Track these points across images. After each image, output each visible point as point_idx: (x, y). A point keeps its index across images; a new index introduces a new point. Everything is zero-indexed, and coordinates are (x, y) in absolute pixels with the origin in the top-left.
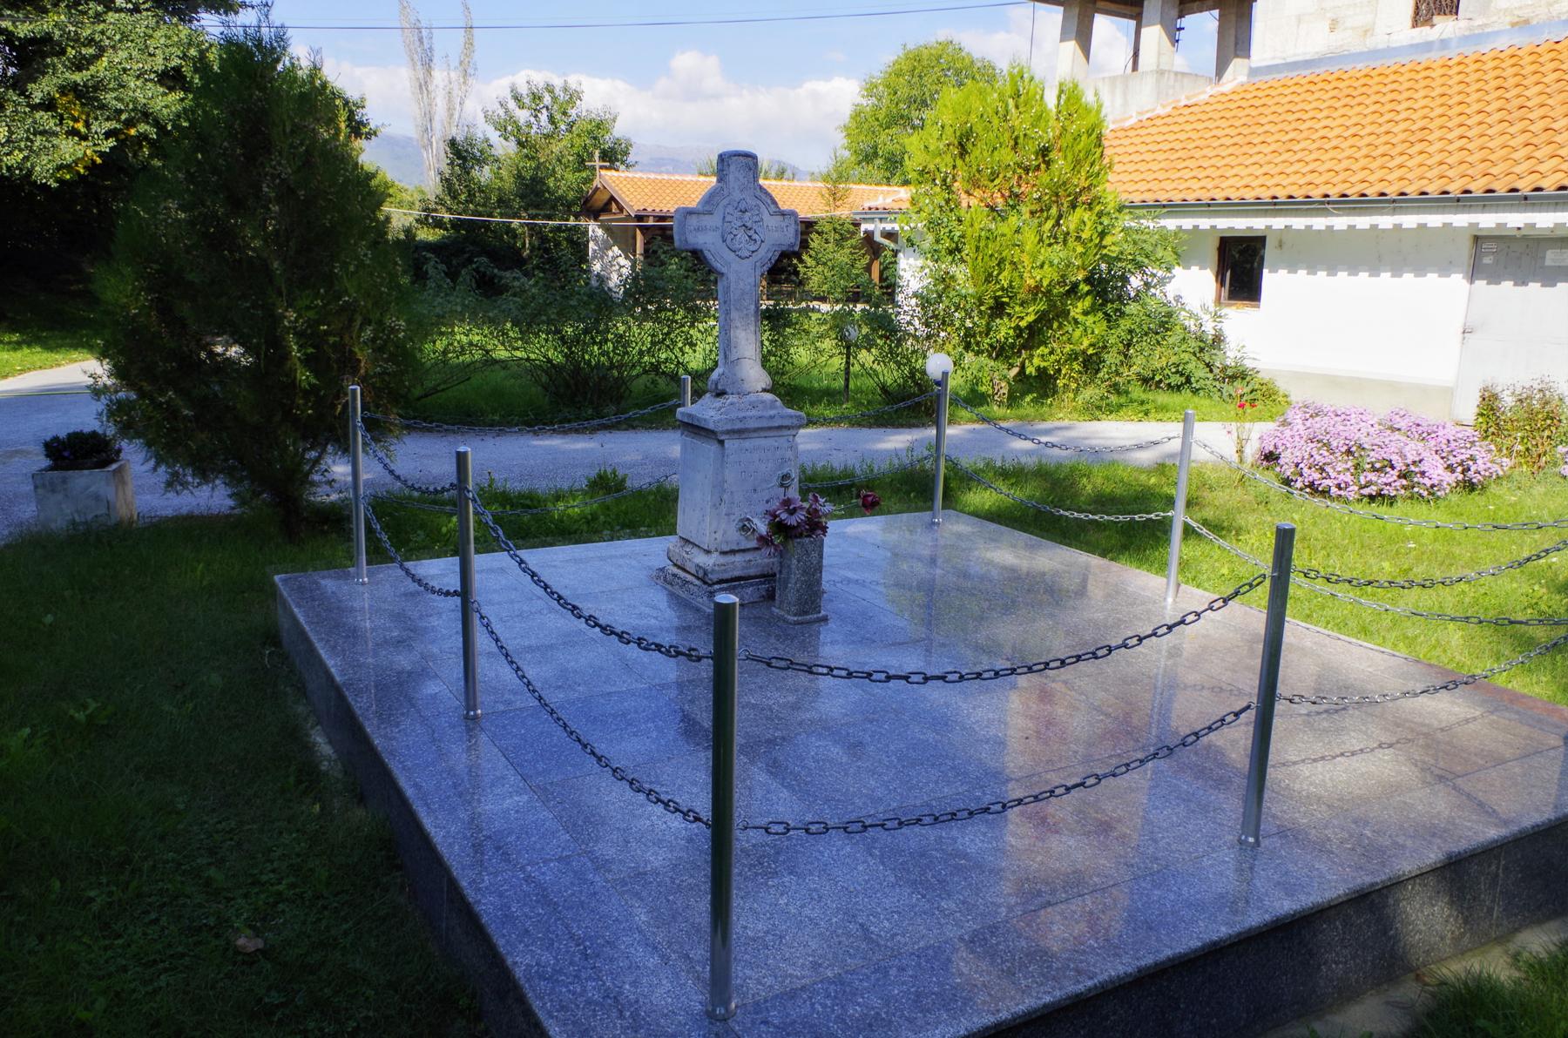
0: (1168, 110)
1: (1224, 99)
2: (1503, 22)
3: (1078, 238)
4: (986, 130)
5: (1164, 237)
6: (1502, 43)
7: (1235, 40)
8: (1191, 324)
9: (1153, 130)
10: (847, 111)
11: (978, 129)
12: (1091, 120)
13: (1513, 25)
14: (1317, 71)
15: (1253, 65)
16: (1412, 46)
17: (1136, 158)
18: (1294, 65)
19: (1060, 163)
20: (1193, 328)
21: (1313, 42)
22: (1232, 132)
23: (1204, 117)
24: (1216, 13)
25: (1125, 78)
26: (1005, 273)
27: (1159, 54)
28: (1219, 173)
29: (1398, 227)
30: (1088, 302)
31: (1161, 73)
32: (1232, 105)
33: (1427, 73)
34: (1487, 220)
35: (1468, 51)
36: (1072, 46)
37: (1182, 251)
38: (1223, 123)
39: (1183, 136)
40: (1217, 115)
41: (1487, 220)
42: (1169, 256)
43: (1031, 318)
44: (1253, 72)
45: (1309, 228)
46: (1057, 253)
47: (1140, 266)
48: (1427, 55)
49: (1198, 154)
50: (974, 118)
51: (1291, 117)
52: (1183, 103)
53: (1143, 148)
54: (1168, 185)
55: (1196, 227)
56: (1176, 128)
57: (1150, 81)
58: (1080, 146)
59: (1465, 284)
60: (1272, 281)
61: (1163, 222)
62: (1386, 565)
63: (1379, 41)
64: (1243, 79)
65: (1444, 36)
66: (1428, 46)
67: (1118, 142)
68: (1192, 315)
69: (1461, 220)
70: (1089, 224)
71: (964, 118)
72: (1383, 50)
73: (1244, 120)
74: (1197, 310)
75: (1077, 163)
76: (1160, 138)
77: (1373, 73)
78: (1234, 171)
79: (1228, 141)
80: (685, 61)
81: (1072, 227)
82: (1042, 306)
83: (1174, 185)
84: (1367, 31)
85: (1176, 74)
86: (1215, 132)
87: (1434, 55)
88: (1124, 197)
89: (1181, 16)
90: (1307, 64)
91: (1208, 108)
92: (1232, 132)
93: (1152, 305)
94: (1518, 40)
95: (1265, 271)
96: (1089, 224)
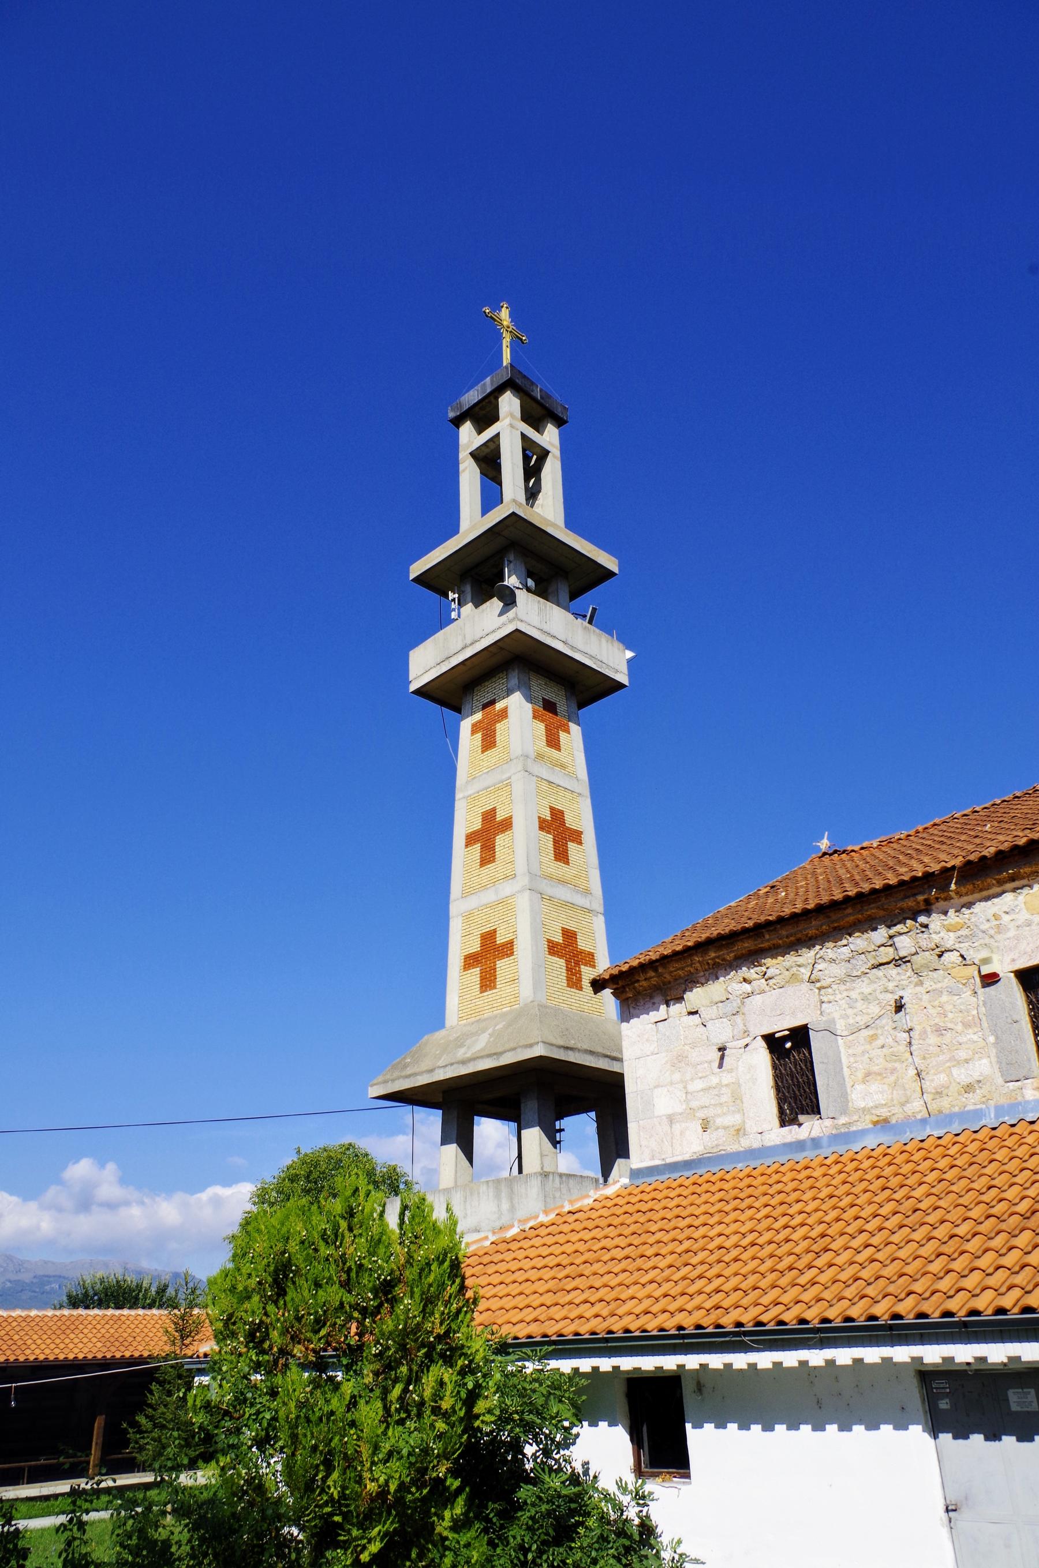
0: (552, 1216)
1: (610, 1204)
2: (865, 1124)
3: (436, 1411)
4: (309, 1260)
5: (557, 1384)
6: (871, 1142)
7: (614, 1143)
8: (607, 1508)
9: (537, 1242)
10: (238, 1217)
11: (299, 1260)
12: (444, 1242)
13: (875, 1123)
14: (700, 1172)
15: (634, 1166)
16: (785, 1145)
17: (520, 1276)
18: (673, 1167)
19: (408, 1303)
20: (613, 1516)
21: (691, 1144)
22: (622, 1242)
23: (590, 1224)
24: (593, 1114)
25: (510, 1181)
26: (335, 1475)
27: (542, 1156)
28: (613, 1294)
29: (831, 1363)
30: (459, 1508)
31: (545, 1175)
32: (618, 1211)
33: (808, 1172)
34: (933, 1354)
35: (841, 1149)
36: (452, 1150)
37: (589, 1401)
38: (611, 1231)
39: (569, 1248)
40: (603, 1223)
41: (933, 1354)
42: (565, 1410)
43: (375, 1548)
44: (635, 1174)
45: (728, 1366)
46: (405, 1438)
47: (529, 1428)
48: (805, 1154)
49: (587, 1270)
50: (293, 1246)
51: (682, 1224)
52: (567, 1209)
53: (527, 1264)
54: (557, 1313)
55: (595, 1369)
56: (561, 1239)
57: (535, 1184)
58: (431, 1279)
59: (927, 1437)
60: (702, 1440)
61: (553, 1364)
62: (645, 984)
63: (751, 1141)
64: (625, 1181)
65: (814, 1134)
66: (799, 1146)
67: (500, 1257)
68: (607, 1497)
69: (902, 1354)
70: (450, 1387)
71: (280, 1246)
72: (759, 1149)
73: (633, 1228)
74: (613, 1489)
75: (428, 1302)
76: (545, 1251)
77: (755, 1173)
78: (631, 1292)
79: (618, 1253)
80: (82, 1169)
81: (428, 1393)
82: (390, 1525)
83: (564, 1312)
84: (739, 1131)
85: (561, 1175)
86: (605, 1243)
87: (810, 1154)
88: (505, 1330)
89: (560, 1117)
90: (687, 1164)
91: (594, 1214)
92: (622, 1242)
93: (555, 1483)
94: (886, 1139)
95: (688, 1426)
96: (450, 1387)
